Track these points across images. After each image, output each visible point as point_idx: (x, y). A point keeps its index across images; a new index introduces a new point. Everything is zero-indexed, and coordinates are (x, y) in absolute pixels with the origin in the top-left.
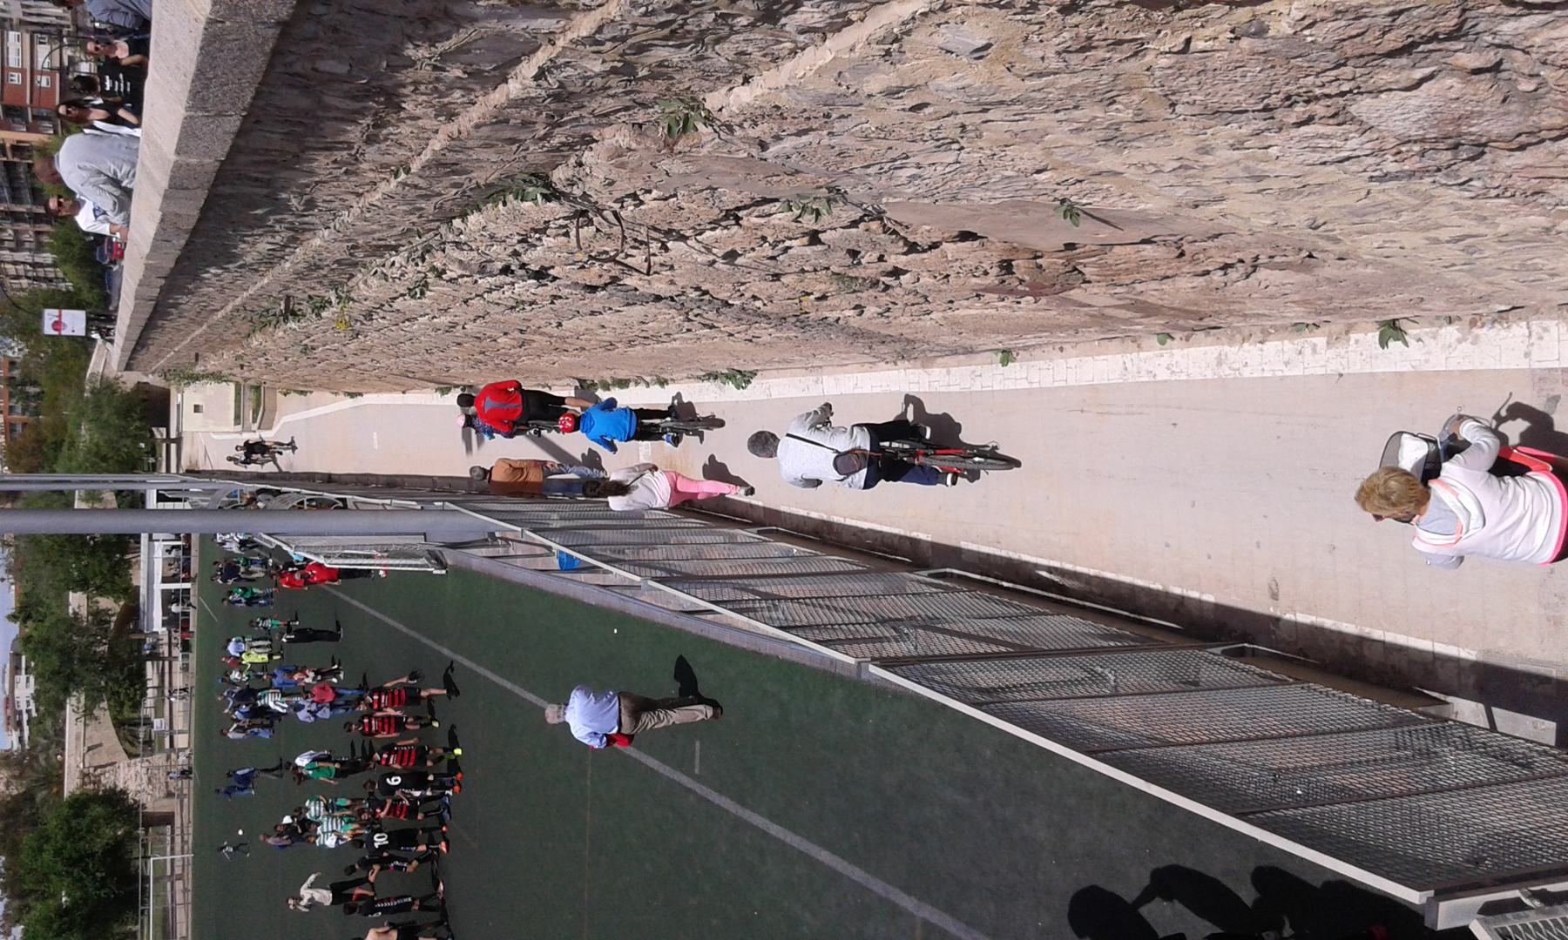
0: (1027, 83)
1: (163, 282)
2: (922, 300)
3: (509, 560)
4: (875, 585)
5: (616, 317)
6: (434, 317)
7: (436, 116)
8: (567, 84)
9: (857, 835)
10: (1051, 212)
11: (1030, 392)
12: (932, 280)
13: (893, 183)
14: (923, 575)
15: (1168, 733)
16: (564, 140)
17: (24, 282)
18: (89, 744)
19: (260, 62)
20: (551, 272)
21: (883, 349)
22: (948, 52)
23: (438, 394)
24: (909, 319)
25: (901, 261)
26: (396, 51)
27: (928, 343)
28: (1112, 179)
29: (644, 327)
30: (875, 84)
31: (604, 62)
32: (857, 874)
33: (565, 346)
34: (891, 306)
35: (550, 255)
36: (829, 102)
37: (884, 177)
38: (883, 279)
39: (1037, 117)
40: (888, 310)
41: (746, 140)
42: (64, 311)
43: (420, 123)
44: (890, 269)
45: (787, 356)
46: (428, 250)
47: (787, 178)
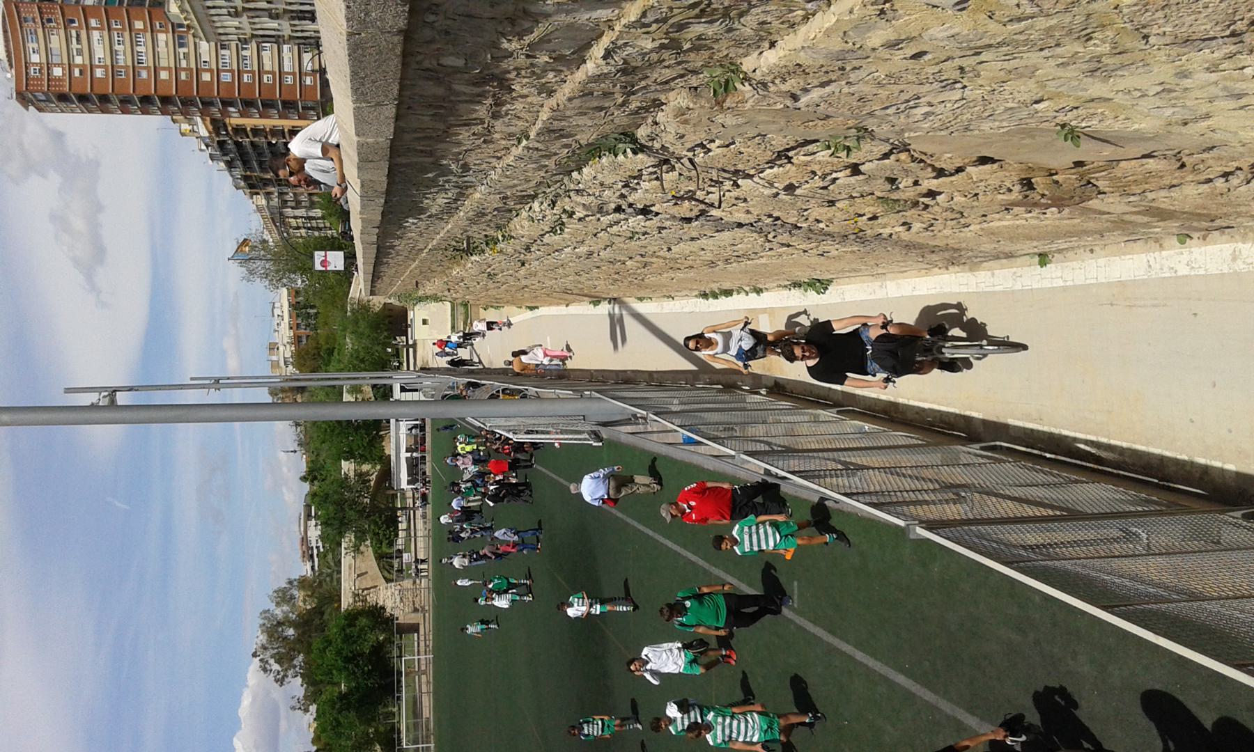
0: (1009, 27)
1: (377, 230)
2: (958, 216)
3: (648, 436)
4: (933, 457)
5: (711, 241)
6: (575, 248)
7: (539, 94)
8: (630, 60)
9: (927, 663)
10: (1055, 136)
11: (1065, 289)
12: (964, 199)
13: (911, 120)
14: (975, 448)
15: (1196, 586)
16: (639, 105)
17: (303, 231)
18: (358, 572)
19: (394, 65)
20: (653, 209)
21: (934, 257)
22: (934, 6)
23: (592, 306)
24: (950, 232)
25: (934, 184)
26: (495, 45)
27: (972, 250)
28: (1103, 104)
29: (735, 248)
30: (876, 38)
31: (654, 40)
32: (928, 696)
33: (678, 266)
34: (933, 221)
35: (648, 196)
36: (841, 56)
37: (902, 116)
38: (922, 200)
39: (1025, 55)
40: (932, 225)
41: (780, 93)
42: (328, 252)
43: (529, 100)
44: (925, 191)
45: (854, 266)
46: (557, 196)
47: (821, 123)
